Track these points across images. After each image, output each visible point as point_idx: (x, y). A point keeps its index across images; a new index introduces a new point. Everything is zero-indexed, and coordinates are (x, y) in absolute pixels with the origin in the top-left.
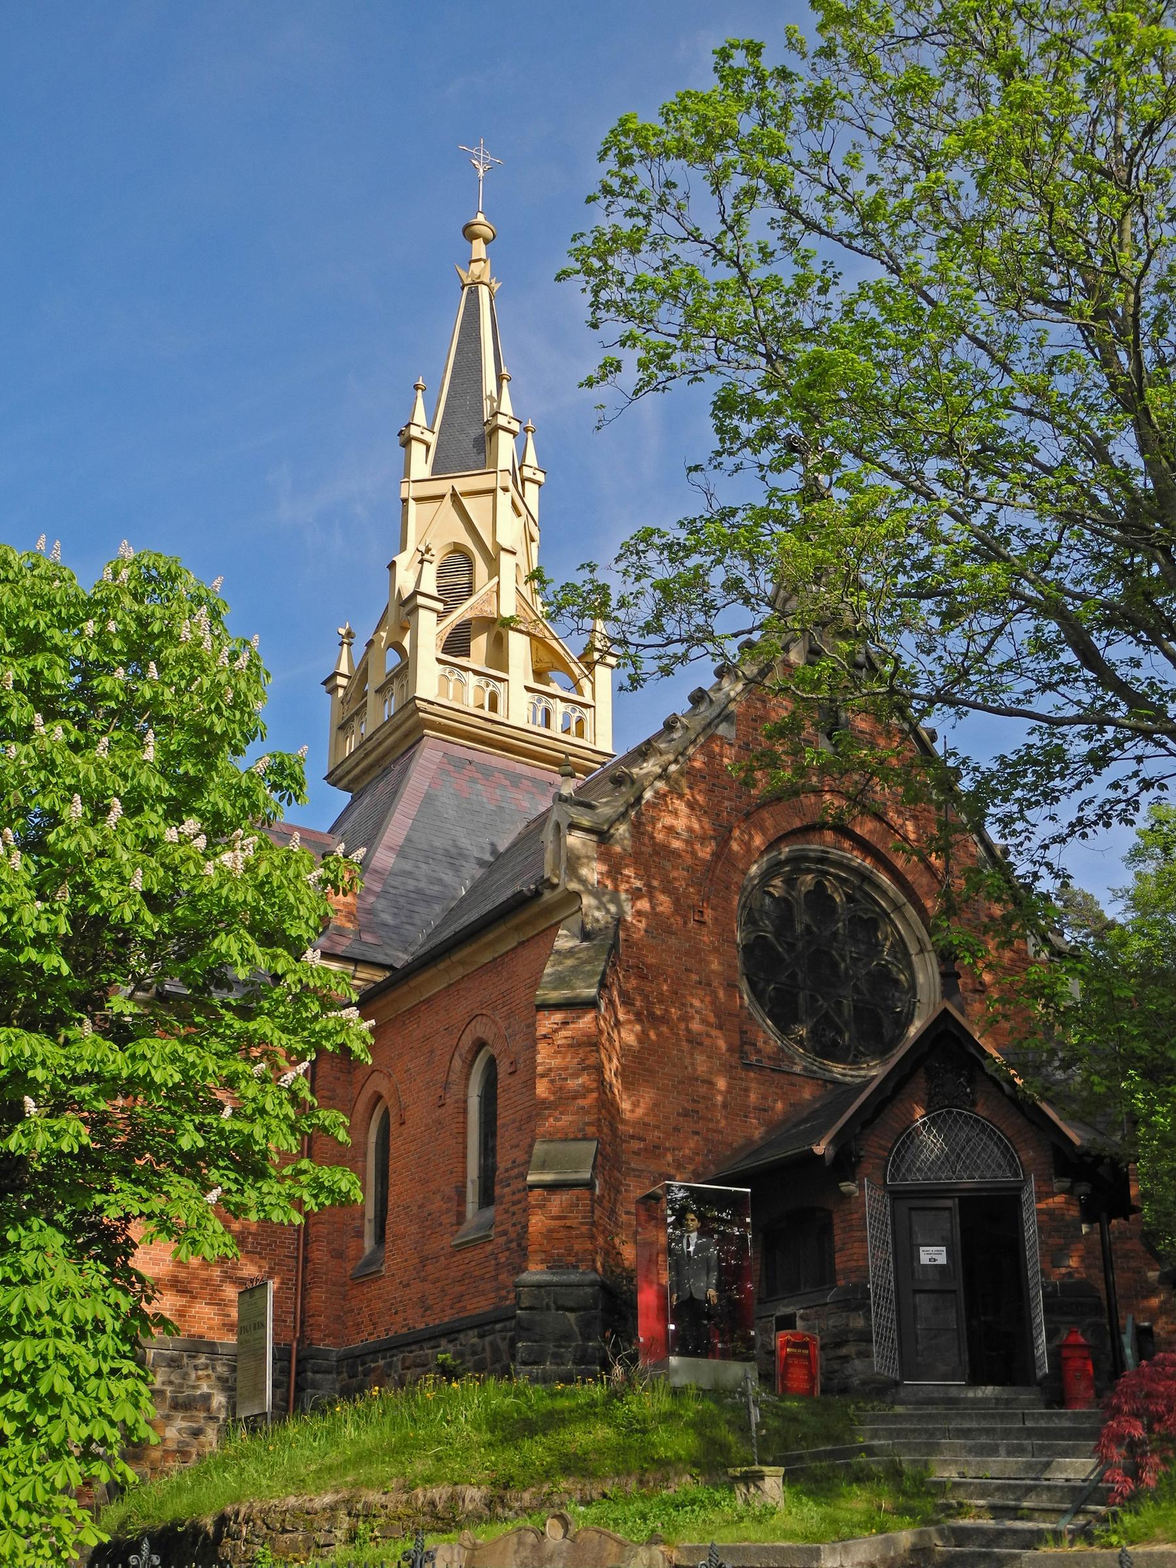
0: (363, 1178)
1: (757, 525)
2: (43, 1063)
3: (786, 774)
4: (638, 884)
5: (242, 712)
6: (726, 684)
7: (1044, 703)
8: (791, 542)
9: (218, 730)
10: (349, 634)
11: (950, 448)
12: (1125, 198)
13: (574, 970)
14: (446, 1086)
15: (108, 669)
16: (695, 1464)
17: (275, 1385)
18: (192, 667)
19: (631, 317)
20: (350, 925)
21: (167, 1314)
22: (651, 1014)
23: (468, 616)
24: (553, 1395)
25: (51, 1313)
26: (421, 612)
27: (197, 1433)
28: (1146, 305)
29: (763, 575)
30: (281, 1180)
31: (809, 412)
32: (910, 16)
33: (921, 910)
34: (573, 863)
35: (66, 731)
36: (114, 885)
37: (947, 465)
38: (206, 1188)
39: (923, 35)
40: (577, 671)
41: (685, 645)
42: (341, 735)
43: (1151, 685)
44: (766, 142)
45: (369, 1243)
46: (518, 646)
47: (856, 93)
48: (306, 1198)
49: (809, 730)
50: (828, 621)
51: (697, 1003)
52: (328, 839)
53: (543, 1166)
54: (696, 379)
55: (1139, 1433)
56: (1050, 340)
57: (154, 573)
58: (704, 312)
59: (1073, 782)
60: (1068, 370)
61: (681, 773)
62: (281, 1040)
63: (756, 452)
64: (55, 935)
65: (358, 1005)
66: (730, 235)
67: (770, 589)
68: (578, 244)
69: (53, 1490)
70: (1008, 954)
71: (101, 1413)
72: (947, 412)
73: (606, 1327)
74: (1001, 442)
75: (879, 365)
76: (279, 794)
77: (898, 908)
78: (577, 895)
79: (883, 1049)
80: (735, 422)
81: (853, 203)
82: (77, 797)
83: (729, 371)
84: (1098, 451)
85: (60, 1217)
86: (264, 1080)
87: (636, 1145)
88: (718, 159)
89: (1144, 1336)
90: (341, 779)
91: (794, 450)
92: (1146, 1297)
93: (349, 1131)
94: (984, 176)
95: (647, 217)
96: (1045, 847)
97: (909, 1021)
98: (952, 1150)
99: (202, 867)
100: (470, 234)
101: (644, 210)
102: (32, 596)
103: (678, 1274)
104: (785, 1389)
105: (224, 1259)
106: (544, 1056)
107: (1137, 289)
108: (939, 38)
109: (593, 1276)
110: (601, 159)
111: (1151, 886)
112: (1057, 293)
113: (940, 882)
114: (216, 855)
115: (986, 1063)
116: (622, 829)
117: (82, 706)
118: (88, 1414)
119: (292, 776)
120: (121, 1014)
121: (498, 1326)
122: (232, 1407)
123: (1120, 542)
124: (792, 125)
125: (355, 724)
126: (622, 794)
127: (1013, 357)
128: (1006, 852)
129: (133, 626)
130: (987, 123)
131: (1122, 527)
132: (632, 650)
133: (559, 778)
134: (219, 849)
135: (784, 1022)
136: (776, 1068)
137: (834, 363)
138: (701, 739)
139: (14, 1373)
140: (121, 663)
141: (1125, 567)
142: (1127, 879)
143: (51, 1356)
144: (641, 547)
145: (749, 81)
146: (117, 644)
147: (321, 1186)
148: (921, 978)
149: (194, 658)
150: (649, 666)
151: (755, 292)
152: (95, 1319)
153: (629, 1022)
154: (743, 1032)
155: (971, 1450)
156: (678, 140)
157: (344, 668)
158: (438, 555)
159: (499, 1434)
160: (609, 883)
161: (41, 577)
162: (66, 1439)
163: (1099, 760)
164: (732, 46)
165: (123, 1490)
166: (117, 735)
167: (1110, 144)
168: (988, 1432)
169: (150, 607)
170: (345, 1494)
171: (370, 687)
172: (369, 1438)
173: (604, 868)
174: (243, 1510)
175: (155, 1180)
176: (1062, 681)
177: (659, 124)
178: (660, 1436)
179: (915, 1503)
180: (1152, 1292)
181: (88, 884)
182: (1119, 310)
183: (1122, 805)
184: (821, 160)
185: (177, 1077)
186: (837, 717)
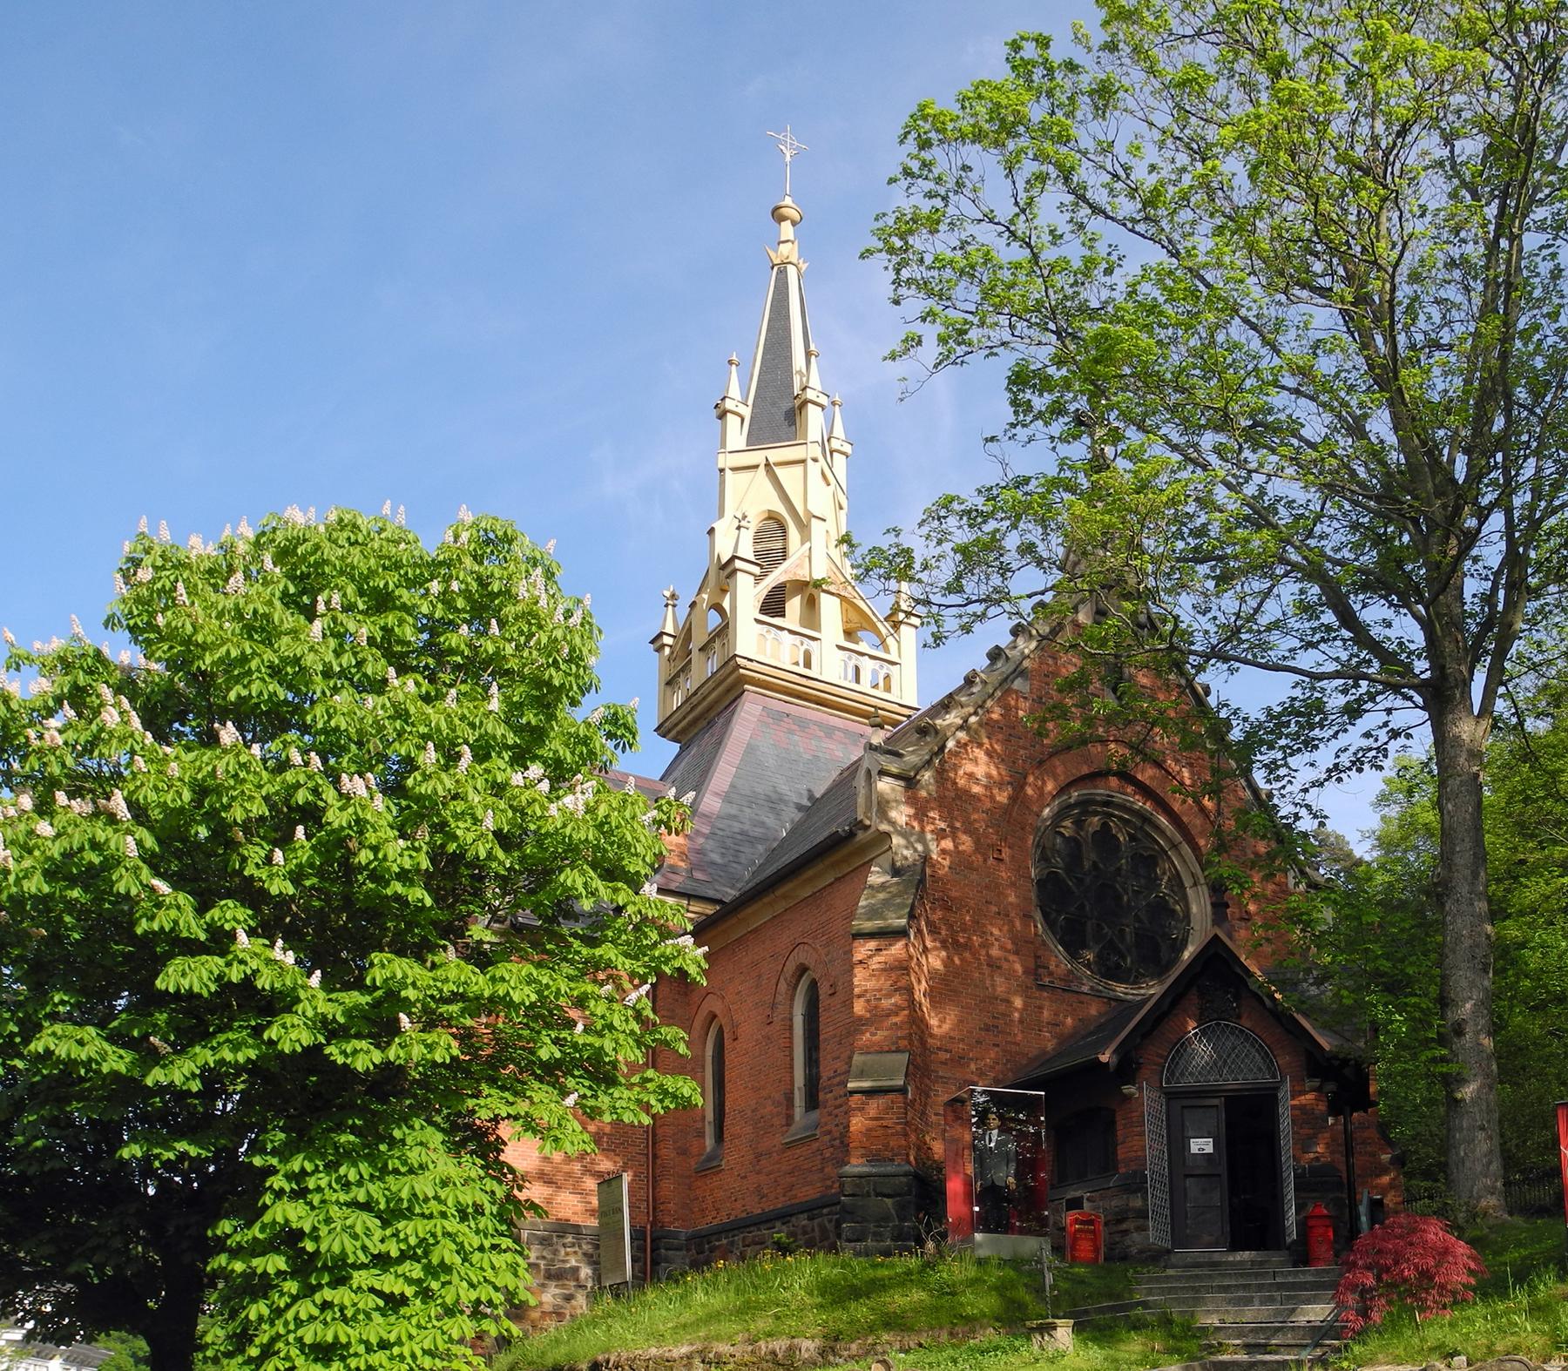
0: (702, 1085)
1: (1049, 491)
2: (414, 984)
3: (1076, 725)
4: (943, 825)
5: (578, 666)
6: (1021, 642)
7: (1307, 660)
8: (1080, 507)
9: (556, 683)
10: (673, 596)
11: (1224, 422)
12: (1382, 192)
13: (885, 902)
14: (773, 1006)
15: (452, 626)
16: (997, 1319)
17: (634, 1260)
18: (530, 624)
19: (930, 294)
20: (682, 864)
21: (537, 1201)
22: (956, 942)
23: (783, 579)
24: (875, 1266)
25: (436, 1198)
26: (739, 574)
27: (569, 1298)
28: (1399, 294)
29: (1056, 539)
30: (630, 1087)
31: (1096, 386)
32: (1186, 15)
33: (1195, 848)
34: (883, 806)
35: (417, 684)
36: (468, 825)
37: (1221, 438)
38: (564, 1093)
39: (1199, 33)
40: (884, 631)
41: (984, 605)
42: (669, 690)
43: (1401, 644)
44: (1056, 129)
45: (709, 1142)
46: (830, 608)
47: (1137, 87)
48: (653, 1102)
49: (1096, 685)
50: (1113, 584)
51: (996, 932)
52: (660, 786)
53: (861, 1075)
54: (992, 354)
55: (1370, 1281)
56: (1315, 324)
57: (492, 536)
58: (998, 290)
59: (1331, 732)
60: (1331, 351)
61: (980, 723)
62: (624, 965)
63: (1047, 424)
64: (418, 871)
65: (692, 934)
66: (1023, 217)
67: (1061, 551)
68: (880, 224)
69: (451, 1341)
70: (1271, 887)
71: (486, 1280)
72: (1222, 389)
73: (919, 1209)
74: (1270, 419)
75: (1160, 343)
76: (614, 742)
77: (1175, 846)
78: (888, 835)
79: (1160, 970)
80: (1028, 396)
81: (1136, 190)
82: (430, 745)
83: (1021, 347)
84: (1357, 429)
85: (438, 1119)
86: (610, 1000)
87: (944, 1056)
88: (1011, 145)
89: (1376, 1206)
90: (669, 731)
91: (1082, 423)
92: (1379, 1176)
93: (688, 1044)
94: (1255, 167)
95: (945, 199)
96: (1306, 791)
97: (1184, 946)
98: (1220, 1057)
99: (547, 809)
100: (778, 216)
101: (942, 192)
102: (380, 557)
103: (981, 1165)
104: (1074, 1258)
105: (583, 1155)
106: (860, 979)
107: (1393, 277)
108: (1212, 38)
109: (907, 1168)
110: (902, 142)
111: (1394, 828)
112: (1321, 281)
113: (1212, 823)
114: (558, 798)
115: (1250, 981)
116: (927, 776)
117: (431, 661)
118: (475, 1281)
119: (625, 726)
120: (481, 942)
121: (825, 1211)
122: (598, 1277)
123: (1378, 514)
124: (1079, 115)
125: (681, 680)
126: (927, 743)
127: (1281, 339)
128: (1270, 795)
129: (474, 586)
130: (1258, 117)
131: (1378, 499)
132: (935, 609)
133: (870, 730)
134: (561, 792)
135: (1073, 947)
136: (1065, 988)
137: (1119, 340)
138: (999, 693)
139: (409, 1246)
140: (465, 621)
141: (1380, 536)
142: (1373, 822)
143: (439, 1234)
144: (942, 513)
145: (1039, 72)
146: (460, 603)
147: (666, 1092)
148: (1194, 909)
149: (531, 616)
150: (951, 624)
151: (1046, 272)
152: (474, 1204)
153: (935, 948)
154: (1037, 957)
155: (1229, 1302)
156: (973, 126)
157: (669, 629)
158: (754, 524)
159: (829, 1298)
160: (915, 824)
161: (388, 540)
162: (457, 1301)
163: (1353, 712)
164: (1022, 38)
165: (509, 1343)
166: (464, 688)
167: (1369, 143)
168: (1245, 1287)
169: (489, 567)
170: (698, 1346)
171: (694, 646)
172: (717, 1301)
173: (911, 811)
174: (613, 1359)
175: (519, 1087)
176: (1323, 640)
177: (955, 109)
178: (968, 1297)
179: (1184, 1345)
180: (1385, 1171)
181: (444, 824)
182: (1376, 298)
183: (1373, 753)
184: (1107, 148)
185: (534, 997)
186: (1121, 673)
